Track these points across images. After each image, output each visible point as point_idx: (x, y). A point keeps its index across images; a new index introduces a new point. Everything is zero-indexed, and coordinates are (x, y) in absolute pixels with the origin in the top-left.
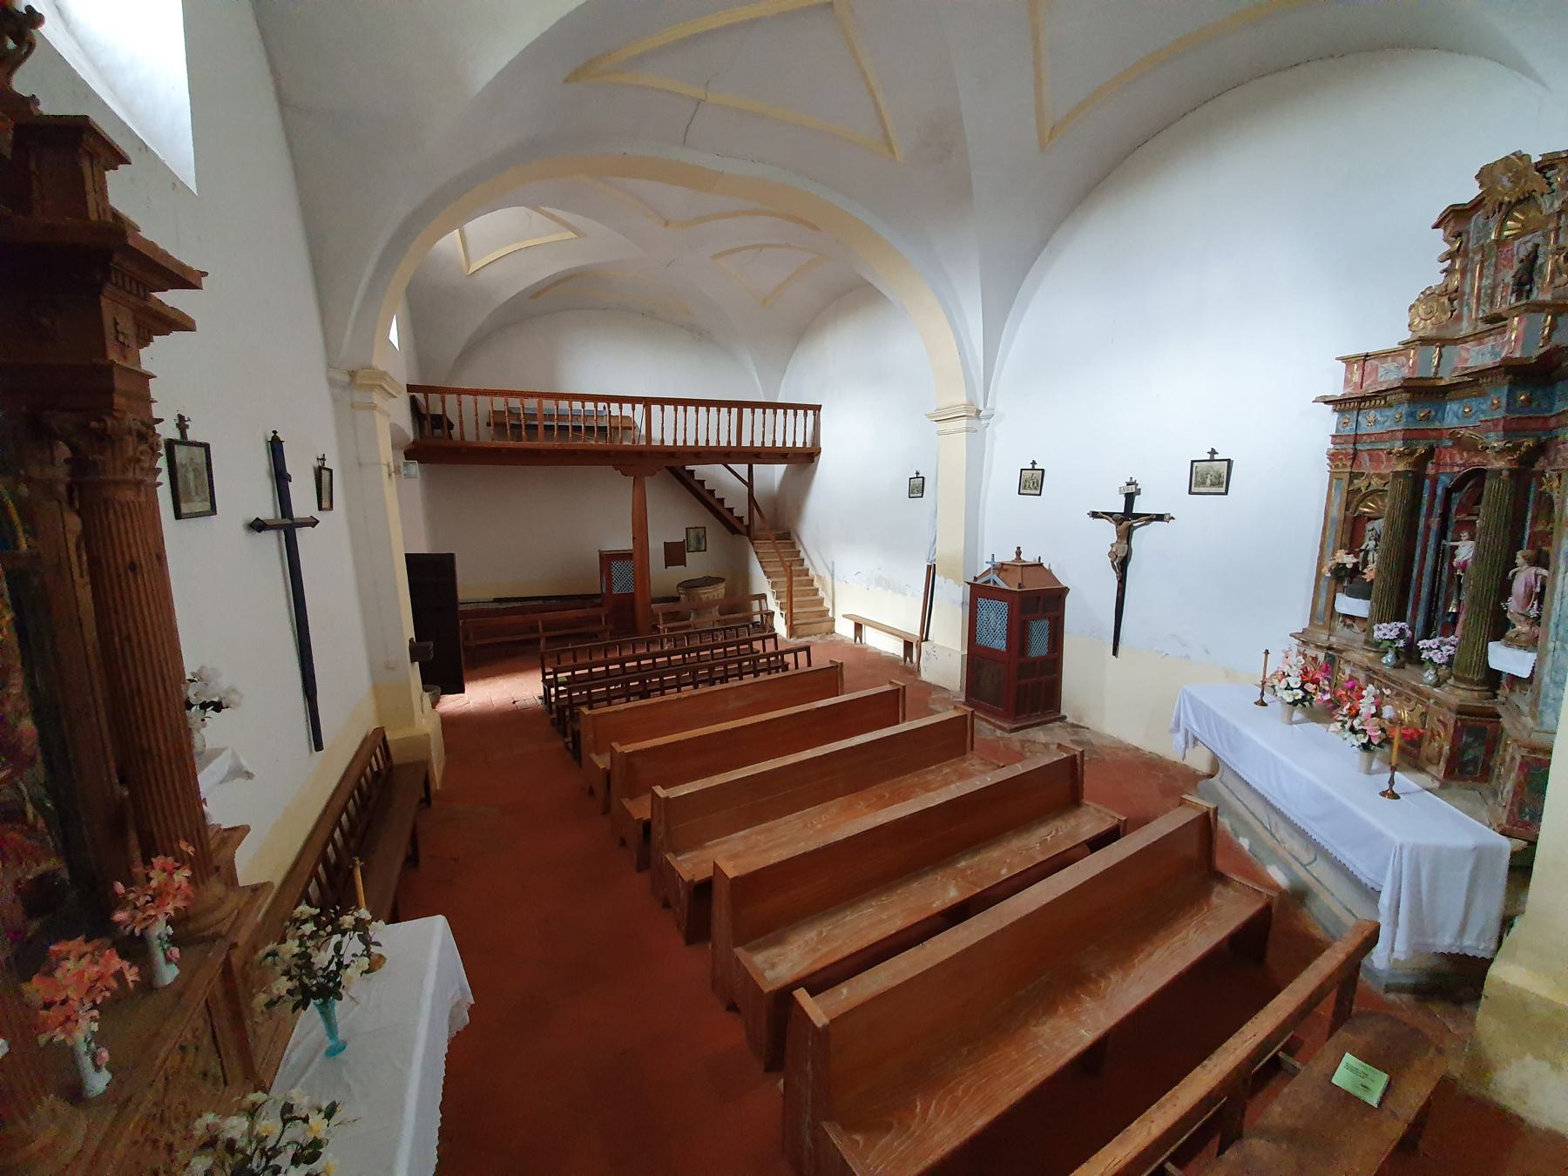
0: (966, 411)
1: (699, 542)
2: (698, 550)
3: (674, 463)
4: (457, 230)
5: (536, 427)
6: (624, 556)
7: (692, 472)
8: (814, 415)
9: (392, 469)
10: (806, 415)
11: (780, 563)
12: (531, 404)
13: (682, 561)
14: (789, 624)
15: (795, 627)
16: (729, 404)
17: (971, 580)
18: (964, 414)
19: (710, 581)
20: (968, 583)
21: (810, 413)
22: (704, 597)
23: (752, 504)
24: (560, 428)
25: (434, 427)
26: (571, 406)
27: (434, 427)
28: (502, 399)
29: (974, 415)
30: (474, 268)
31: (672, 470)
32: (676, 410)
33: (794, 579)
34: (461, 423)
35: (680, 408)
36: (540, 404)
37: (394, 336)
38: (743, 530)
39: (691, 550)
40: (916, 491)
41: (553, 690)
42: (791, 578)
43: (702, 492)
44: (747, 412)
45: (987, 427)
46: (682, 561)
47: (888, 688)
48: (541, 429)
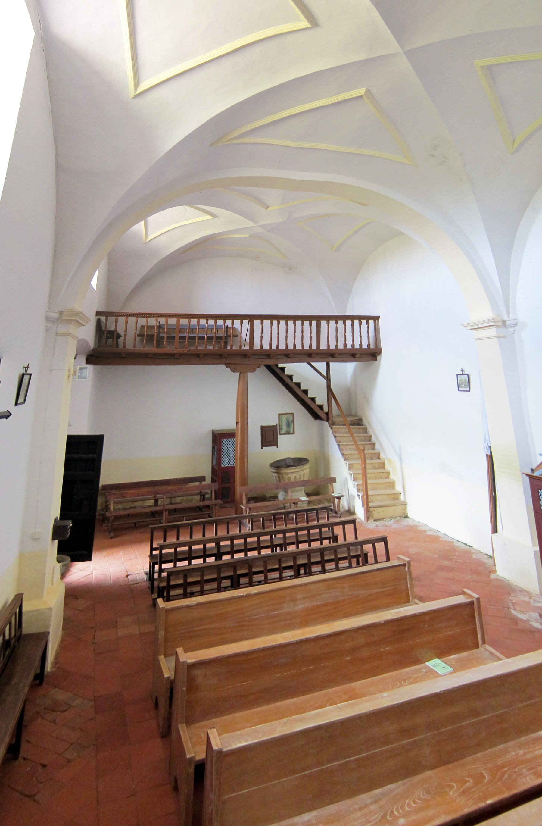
0: (494, 322)
1: (288, 425)
2: (288, 433)
3: (271, 362)
4: (311, 26)
5: (174, 338)
6: (231, 435)
7: (283, 369)
8: (375, 323)
9: (72, 373)
10: (368, 324)
11: (354, 447)
12: (173, 321)
13: (274, 443)
14: (366, 507)
15: (371, 509)
16: (310, 318)
17: (529, 472)
18: (493, 324)
19: (300, 462)
20: (527, 475)
21: (372, 322)
22: (292, 476)
23: (330, 394)
24: (190, 338)
25: (108, 338)
26: (198, 322)
27: (108, 338)
28: (154, 319)
29: (501, 324)
30: (149, 239)
31: (268, 367)
32: (272, 323)
33: (368, 461)
34: (125, 335)
35: (275, 322)
36: (178, 322)
37: (94, 283)
38: (324, 416)
39: (282, 433)
40: (463, 385)
41: (157, 567)
42: (365, 461)
43: (291, 384)
44: (323, 323)
45: (514, 333)
46: (274, 443)
47: (460, 599)
48: (177, 339)
